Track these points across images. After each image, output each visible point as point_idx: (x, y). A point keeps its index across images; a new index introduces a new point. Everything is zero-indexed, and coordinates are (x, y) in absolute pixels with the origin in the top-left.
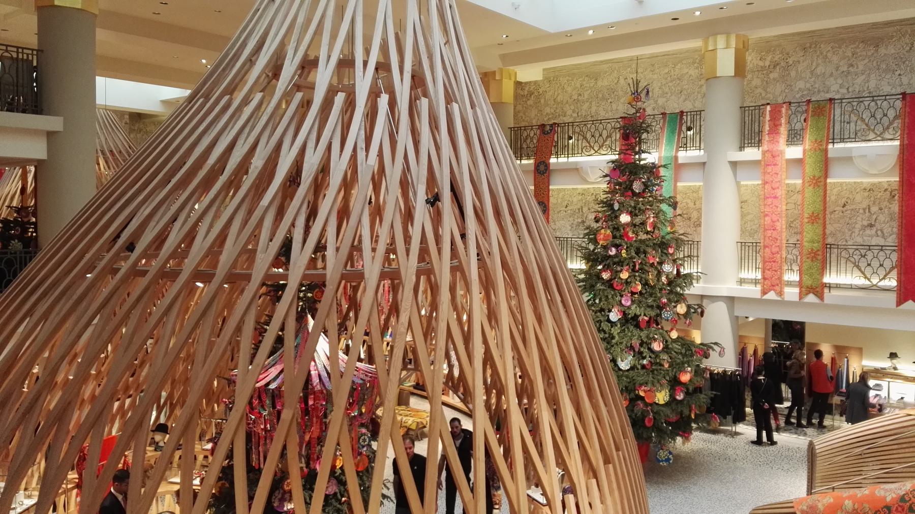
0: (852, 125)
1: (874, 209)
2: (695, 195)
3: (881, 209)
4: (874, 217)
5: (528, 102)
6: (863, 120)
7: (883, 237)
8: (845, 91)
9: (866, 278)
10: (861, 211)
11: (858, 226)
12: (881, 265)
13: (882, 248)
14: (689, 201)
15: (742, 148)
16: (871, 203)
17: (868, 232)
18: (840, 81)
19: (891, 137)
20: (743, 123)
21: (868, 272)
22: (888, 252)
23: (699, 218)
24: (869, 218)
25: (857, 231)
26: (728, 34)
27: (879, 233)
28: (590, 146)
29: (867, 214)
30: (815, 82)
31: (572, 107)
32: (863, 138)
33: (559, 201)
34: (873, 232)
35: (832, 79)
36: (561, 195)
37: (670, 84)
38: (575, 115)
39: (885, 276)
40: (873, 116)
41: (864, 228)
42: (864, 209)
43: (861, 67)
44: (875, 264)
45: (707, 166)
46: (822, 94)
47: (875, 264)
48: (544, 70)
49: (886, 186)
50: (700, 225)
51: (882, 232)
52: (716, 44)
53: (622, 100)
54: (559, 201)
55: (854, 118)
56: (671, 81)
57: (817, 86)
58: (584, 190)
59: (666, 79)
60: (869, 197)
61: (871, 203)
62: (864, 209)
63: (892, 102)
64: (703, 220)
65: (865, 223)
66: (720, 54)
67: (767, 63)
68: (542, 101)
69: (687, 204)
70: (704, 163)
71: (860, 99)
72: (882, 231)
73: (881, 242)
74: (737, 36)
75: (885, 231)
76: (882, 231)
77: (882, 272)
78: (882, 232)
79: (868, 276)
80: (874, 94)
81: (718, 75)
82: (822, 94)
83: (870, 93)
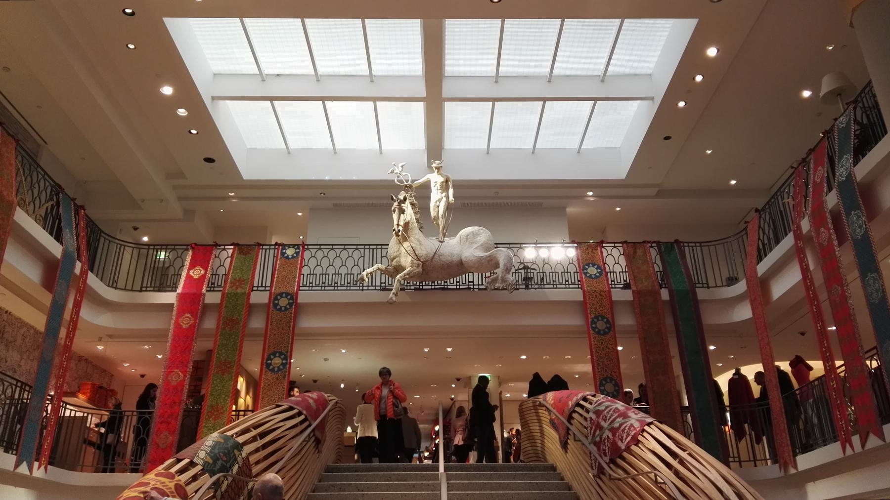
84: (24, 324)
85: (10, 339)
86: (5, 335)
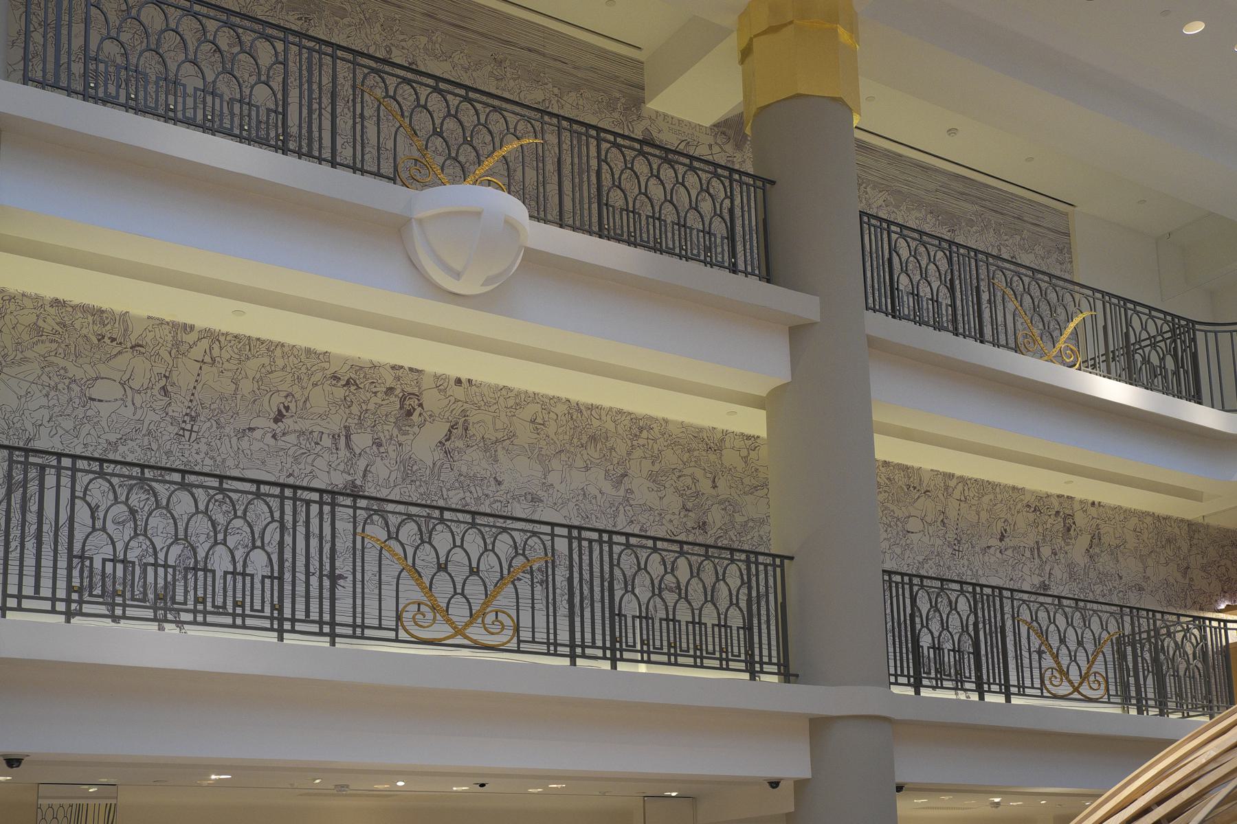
4: (1047, 568)
16: (352, 422)
24: (1041, 568)
42: (1032, 550)
60: (346, 403)
61: (352, 422)
69: (695, 481)
84: (1128, 513)
85: (1114, 543)
86: (1105, 539)
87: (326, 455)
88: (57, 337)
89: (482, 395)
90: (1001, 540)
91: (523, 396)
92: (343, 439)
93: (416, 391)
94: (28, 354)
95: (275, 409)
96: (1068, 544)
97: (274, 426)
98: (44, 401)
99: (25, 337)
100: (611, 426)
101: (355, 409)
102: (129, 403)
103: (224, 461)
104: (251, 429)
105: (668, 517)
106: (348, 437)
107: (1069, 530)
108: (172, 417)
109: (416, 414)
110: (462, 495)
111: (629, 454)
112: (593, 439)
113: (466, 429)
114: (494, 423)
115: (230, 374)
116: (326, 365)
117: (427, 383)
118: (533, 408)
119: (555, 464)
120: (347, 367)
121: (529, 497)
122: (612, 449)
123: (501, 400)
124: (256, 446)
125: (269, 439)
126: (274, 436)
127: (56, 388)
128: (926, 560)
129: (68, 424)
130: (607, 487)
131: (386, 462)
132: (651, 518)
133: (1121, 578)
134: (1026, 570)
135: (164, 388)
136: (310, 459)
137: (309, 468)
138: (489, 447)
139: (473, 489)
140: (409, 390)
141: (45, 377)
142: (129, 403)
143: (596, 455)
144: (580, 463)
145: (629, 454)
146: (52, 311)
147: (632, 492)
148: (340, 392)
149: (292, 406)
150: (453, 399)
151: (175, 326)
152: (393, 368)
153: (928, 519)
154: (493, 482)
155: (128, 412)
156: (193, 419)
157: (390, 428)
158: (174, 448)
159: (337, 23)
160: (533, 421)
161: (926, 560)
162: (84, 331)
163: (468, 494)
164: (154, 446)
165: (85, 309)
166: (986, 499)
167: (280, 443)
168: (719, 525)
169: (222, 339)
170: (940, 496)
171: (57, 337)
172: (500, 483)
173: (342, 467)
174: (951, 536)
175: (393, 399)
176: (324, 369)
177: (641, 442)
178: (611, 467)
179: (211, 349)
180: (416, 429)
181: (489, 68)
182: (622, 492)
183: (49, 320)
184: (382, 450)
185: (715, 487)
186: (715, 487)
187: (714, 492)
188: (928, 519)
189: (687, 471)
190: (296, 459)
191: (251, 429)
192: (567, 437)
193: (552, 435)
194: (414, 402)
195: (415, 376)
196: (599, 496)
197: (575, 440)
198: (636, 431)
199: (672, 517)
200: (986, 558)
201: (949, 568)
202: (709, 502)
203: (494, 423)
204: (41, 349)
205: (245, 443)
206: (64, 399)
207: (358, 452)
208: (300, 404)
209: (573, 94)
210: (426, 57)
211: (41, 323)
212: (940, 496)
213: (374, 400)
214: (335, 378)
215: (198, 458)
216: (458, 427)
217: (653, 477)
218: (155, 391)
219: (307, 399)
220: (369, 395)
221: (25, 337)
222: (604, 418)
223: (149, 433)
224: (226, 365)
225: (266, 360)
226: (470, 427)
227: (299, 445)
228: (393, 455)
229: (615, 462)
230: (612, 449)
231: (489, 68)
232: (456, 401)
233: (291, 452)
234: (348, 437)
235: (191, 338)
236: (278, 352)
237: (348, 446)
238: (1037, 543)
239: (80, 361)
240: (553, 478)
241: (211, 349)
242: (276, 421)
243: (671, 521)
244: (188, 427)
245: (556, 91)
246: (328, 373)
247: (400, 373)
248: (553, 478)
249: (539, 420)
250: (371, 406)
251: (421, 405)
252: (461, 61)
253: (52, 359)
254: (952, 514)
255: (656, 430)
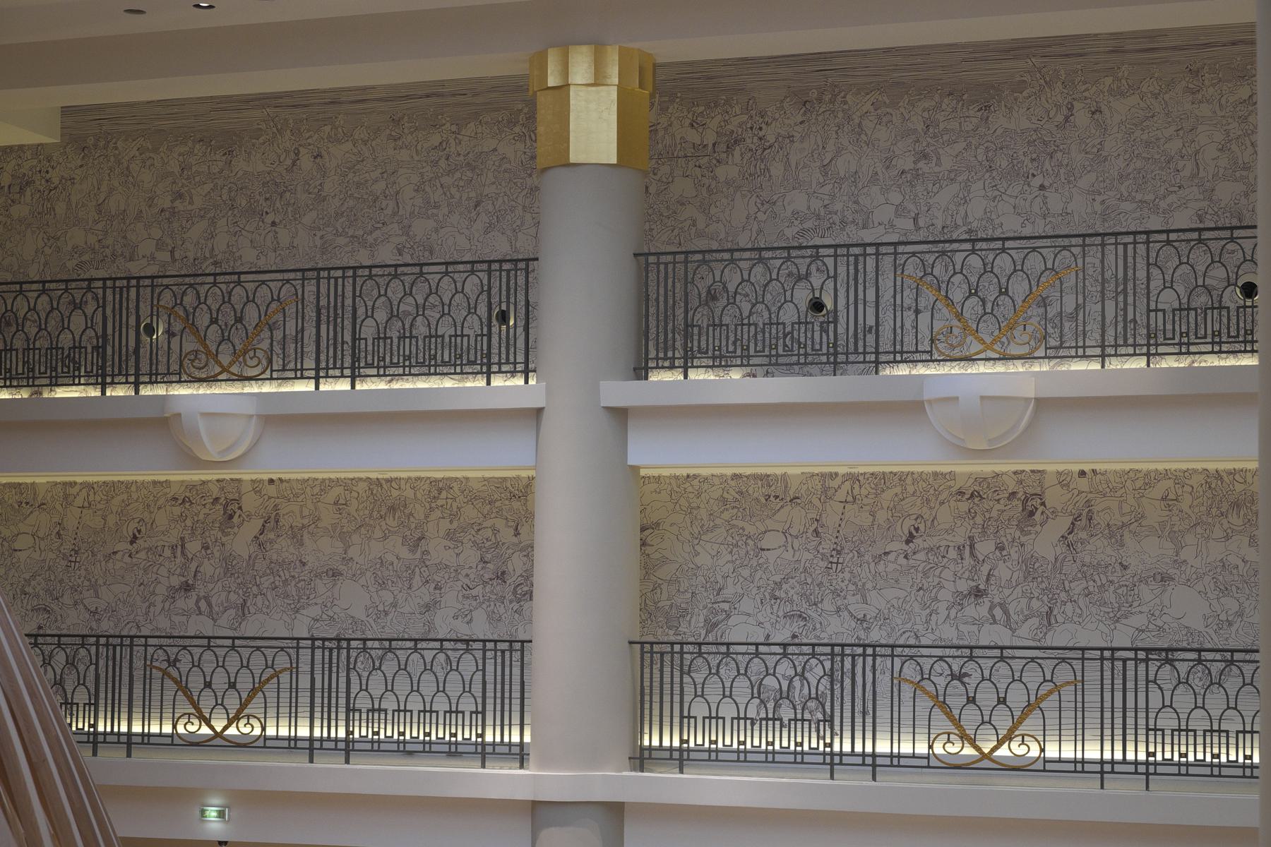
0: (924, 318)
1: (193, 547)
2: (516, 505)
3: (1000, 548)
4: (985, 569)
5: (721, 172)
6: (949, 302)
7: (1008, 624)
8: (909, 225)
9: (964, 737)
10: (168, 553)
11: (161, 590)
12: (1002, 701)
13: (1002, 653)
14: (500, 523)
15: (641, 372)
16: (186, 534)
17: (971, 610)
18: (896, 198)
19: (1024, 350)
20: (643, 299)
21: (970, 718)
22: (1017, 664)
23: (528, 576)
24: (974, 570)
25: (942, 607)
26: (599, 47)
27: (203, 604)
28: (208, 353)
29: (179, 559)
30: (833, 197)
31: (156, 233)
32: (956, 353)
33: (112, 520)
34: (983, 610)
35: (875, 190)
36: (116, 501)
37: (447, 180)
38: (164, 256)
39: (240, 711)
40: (973, 292)
41: (960, 600)
43: (947, 163)
44: (987, 697)
45: (545, 415)
46: (851, 229)
47: (987, 697)
48: (66, 111)
49: (215, 492)
50: (530, 595)
51: (1006, 612)
52: (565, 72)
53: (307, 219)
54: (112, 520)
55: (928, 296)
56: (449, 173)
57: (838, 206)
58: (191, 487)
59: (435, 163)
60: (971, 514)
61: (186, 534)
62: (173, 548)
63: (1018, 256)
64: (537, 579)
65: (964, 586)
66: (577, 99)
67: (710, 138)
68: (60, 208)
69: (495, 531)
70: (539, 411)
71: (942, 244)
72: (1003, 606)
73: (1000, 635)
74: (624, 56)
75: (214, 601)
76: (1003, 606)
77: (1003, 722)
78: (1006, 612)
79: (970, 732)
80: (981, 235)
81: (573, 159)
82: (851, 229)
83: (970, 231)
85: (298, 522)
87: (952, 567)
88: (736, 504)
89: (1108, 482)
90: (132, 543)
91: (1153, 475)
92: (967, 548)
93: (1038, 491)
94: (718, 521)
95: (906, 532)
96: (227, 534)
97: (906, 547)
98: (729, 557)
99: (715, 508)
100: (409, 493)
101: (979, 520)
102: (790, 548)
103: (864, 584)
104: (886, 554)
105: (464, 572)
106: (972, 547)
107: (231, 517)
108: (823, 554)
109: (236, 516)
110: (1084, 585)
111: (426, 517)
112: (392, 509)
113: (277, 522)
114: (301, 512)
115: (868, 508)
116: (952, 483)
117: (246, 488)
118: (338, 490)
119: (1190, 539)
120: (971, 481)
121: (1159, 577)
122: (411, 514)
123: (1129, 483)
124: (891, 567)
125: (902, 560)
126: (906, 557)
127: (737, 546)
128: (785, 579)
129: (746, 573)
130: (404, 553)
131: (1009, 564)
132: (447, 576)
133: (304, 564)
134: (163, 571)
135: (815, 530)
136: (937, 572)
137: (937, 580)
138: (1114, 534)
139: (1096, 578)
140: (231, 496)
141: (729, 539)
142: (790, 548)
143: (394, 524)
144: (378, 534)
145: (426, 517)
146: (733, 483)
147: (428, 552)
148: (964, 506)
149: (922, 527)
150: (1076, 492)
151: (823, 476)
152: (1015, 473)
153: (794, 532)
154: (1118, 567)
155: (788, 555)
156: (839, 553)
157: (1012, 531)
158: (825, 581)
159: (1016, 99)
160: (1164, 499)
161: (785, 579)
162: (756, 495)
163: (1091, 583)
164: (809, 581)
165: (756, 477)
166: (888, 495)
167: (911, 562)
168: (518, 573)
169: (861, 478)
170: (58, 507)
171: (736, 504)
172: (1125, 568)
173: (966, 575)
174: (827, 547)
175: (1015, 502)
176: (950, 487)
177: (440, 502)
178: (408, 533)
179: (852, 488)
180: (1038, 528)
181: (1184, 83)
182: (418, 555)
183: (731, 491)
184: (1004, 553)
185: (517, 534)
186: (517, 534)
187: (515, 540)
188: (794, 532)
189: (488, 523)
190: (925, 573)
191: (886, 554)
192: (367, 512)
193: (1186, 509)
194: (1037, 502)
195: (1038, 476)
196: (1241, 565)
197: (1214, 510)
198: (435, 493)
199: (469, 572)
200: (110, 565)
201: (61, 581)
202: (510, 551)
203: (301, 512)
204: (726, 515)
205: (881, 567)
206: (743, 552)
207: (981, 558)
208: (929, 523)
209: (472, 124)
210: (1111, 99)
211: (726, 495)
212: (58, 507)
213: (998, 507)
214: (961, 493)
215: (843, 585)
216: (271, 521)
217: (450, 535)
218: (809, 535)
219: (935, 518)
220: (991, 503)
221: (715, 508)
222: (403, 487)
223: (805, 570)
224: (866, 501)
225: (898, 490)
226: (1095, 516)
227: (927, 561)
228: (217, 554)
229: (413, 526)
230: (411, 514)
231: (1184, 83)
232: (1080, 493)
233: (920, 569)
234: (972, 547)
235: (835, 484)
236: (909, 480)
237: (972, 554)
238: (182, 539)
239: (754, 519)
240: (353, 552)
241: (852, 488)
242: (908, 542)
243: (467, 575)
244: (835, 560)
245: (454, 128)
246: (953, 490)
247: (1022, 477)
248: (353, 552)
249: (1172, 496)
250: (994, 514)
251: (1043, 504)
252: (1151, 89)
253: (734, 522)
254: (831, 520)
255: (456, 489)
